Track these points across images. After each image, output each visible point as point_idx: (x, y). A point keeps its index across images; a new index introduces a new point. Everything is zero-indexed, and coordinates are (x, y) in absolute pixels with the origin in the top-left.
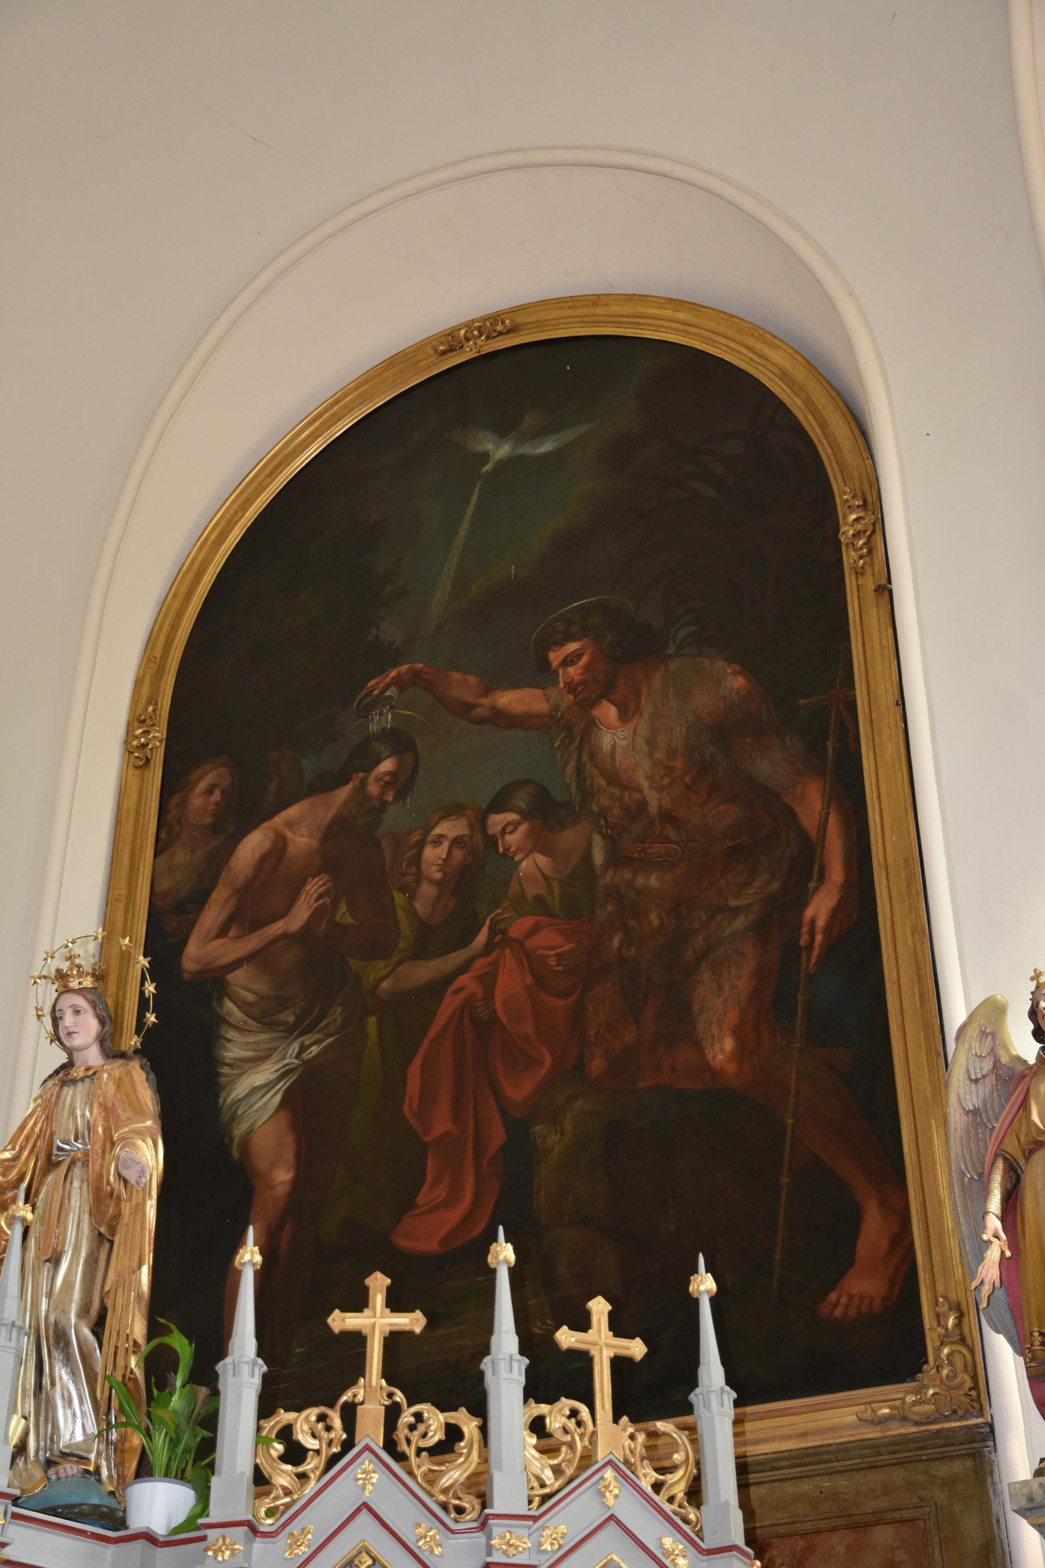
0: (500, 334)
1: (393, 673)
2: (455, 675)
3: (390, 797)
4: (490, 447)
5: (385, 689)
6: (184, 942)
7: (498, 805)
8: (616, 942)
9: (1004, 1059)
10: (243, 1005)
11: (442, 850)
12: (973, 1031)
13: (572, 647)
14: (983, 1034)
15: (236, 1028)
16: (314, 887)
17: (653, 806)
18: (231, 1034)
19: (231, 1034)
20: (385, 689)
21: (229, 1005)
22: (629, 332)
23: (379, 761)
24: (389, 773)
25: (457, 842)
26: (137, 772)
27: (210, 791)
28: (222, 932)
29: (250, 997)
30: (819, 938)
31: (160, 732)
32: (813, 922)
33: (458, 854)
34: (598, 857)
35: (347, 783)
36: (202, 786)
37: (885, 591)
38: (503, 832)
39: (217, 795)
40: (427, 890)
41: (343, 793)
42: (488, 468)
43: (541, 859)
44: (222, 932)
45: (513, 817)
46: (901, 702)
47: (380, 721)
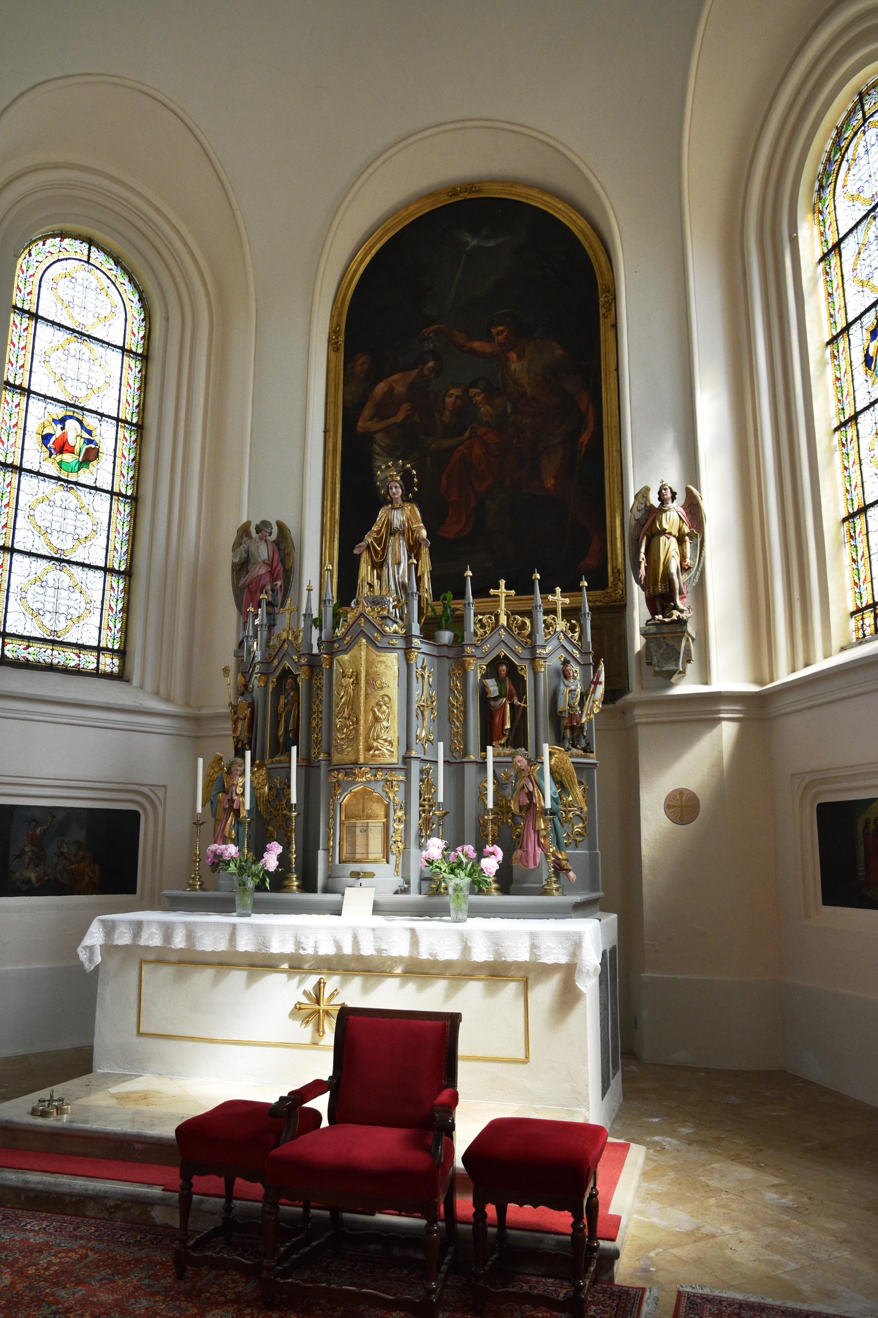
0: (474, 192)
1: (432, 328)
2: (456, 332)
3: (432, 376)
4: (469, 239)
5: (429, 334)
6: (357, 421)
7: (473, 385)
8: (515, 441)
9: (648, 505)
10: (381, 447)
11: (453, 399)
12: (640, 495)
13: (501, 328)
14: (643, 496)
15: (379, 455)
16: (405, 407)
17: (529, 394)
18: (377, 457)
19: (377, 457)
20: (429, 334)
21: (376, 446)
22: (524, 201)
23: (428, 362)
24: (431, 367)
25: (458, 397)
26: (335, 353)
27: (363, 364)
28: (371, 419)
29: (383, 444)
30: (584, 449)
31: (342, 338)
32: (582, 443)
33: (458, 402)
34: (509, 410)
35: (416, 368)
36: (360, 362)
37: (615, 326)
38: (475, 395)
39: (366, 366)
40: (447, 413)
41: (415, 372)
42: (468, 249)
43: (488, 407)
44: (371, 419)
45: (478, 390)
46: (617, 369)
47: (428, 346)
